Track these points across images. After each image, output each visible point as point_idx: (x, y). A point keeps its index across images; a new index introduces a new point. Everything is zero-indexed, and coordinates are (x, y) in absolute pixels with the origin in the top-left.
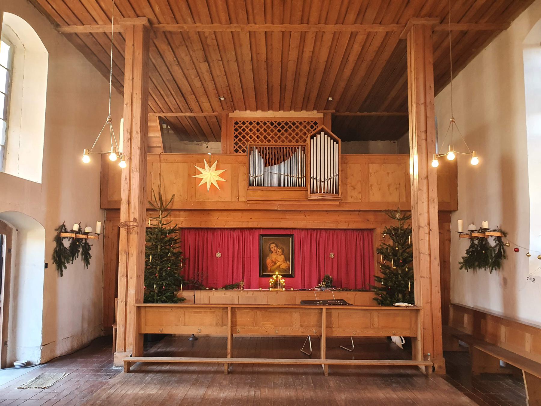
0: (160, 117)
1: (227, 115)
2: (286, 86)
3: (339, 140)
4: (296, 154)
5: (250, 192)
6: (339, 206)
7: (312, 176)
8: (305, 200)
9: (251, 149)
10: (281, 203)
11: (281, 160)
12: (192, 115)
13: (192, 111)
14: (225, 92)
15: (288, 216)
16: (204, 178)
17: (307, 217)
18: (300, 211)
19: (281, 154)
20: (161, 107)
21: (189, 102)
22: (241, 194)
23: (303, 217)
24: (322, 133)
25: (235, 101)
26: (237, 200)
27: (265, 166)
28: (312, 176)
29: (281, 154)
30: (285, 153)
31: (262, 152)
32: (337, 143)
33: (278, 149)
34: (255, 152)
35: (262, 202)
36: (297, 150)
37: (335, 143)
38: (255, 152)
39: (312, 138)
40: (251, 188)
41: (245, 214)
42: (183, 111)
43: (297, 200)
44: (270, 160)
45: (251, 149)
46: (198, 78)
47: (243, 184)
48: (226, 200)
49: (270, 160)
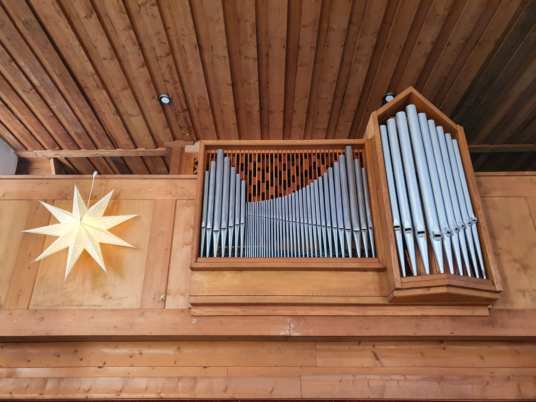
0: (56, 160)
1: (183, 149)
2: (299, 47)
3: (460, 129)
4: (339, 166)
5: (199, 277)
6: (491, 322)
7: (397, 222)
8: (380, 301)
9: (210, 157)
10: (301, 311)
11: (294, 185)
12: (116, 153)
13: (115, 146)
14: (168, 77)
15: (324, 358)
16: (70, 243)
17: (386, 362)
18: (359, 340)
19: (293, 172)
20: (52, 132)
21: (100, 115)
22: (172, 285)
23: (368, 361)
24: (411, 108)
25: (193, 110)
26: (160, 306)
27: (248, 199)
28: (397, 222)
29: (293, 172)
30: (306, 167)
31: (242, 164)
32: (454, 136)
33: (285, 160)
34: (221, 166)
35: (238, 311)
36: (341, 157)
37: (448, 135)
38: (221, 166)
39: (383, 120)
40: (203, 262)
41: (188, 350)
42: (98, 143)
43: (353, 301)
44: (263, 186)
45: (210, 157)
46: (95, 15)
47: (183, 253)
48: (126, 305)
49: (263, 186)
